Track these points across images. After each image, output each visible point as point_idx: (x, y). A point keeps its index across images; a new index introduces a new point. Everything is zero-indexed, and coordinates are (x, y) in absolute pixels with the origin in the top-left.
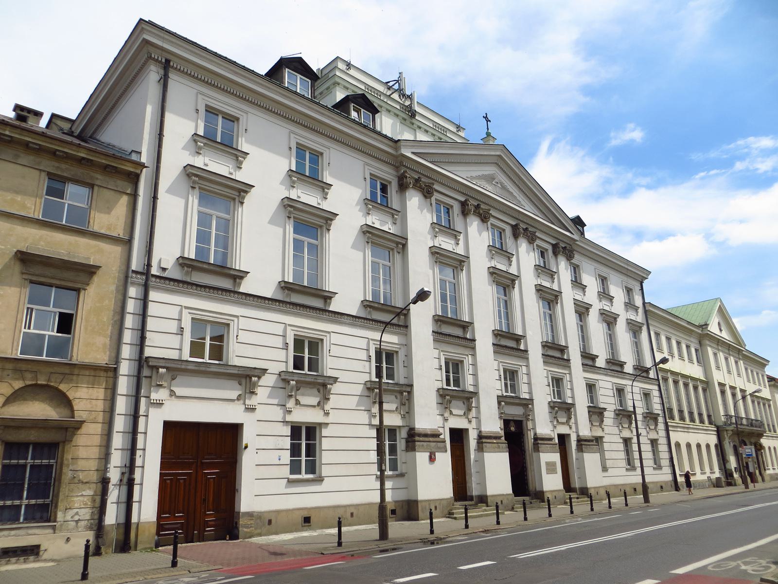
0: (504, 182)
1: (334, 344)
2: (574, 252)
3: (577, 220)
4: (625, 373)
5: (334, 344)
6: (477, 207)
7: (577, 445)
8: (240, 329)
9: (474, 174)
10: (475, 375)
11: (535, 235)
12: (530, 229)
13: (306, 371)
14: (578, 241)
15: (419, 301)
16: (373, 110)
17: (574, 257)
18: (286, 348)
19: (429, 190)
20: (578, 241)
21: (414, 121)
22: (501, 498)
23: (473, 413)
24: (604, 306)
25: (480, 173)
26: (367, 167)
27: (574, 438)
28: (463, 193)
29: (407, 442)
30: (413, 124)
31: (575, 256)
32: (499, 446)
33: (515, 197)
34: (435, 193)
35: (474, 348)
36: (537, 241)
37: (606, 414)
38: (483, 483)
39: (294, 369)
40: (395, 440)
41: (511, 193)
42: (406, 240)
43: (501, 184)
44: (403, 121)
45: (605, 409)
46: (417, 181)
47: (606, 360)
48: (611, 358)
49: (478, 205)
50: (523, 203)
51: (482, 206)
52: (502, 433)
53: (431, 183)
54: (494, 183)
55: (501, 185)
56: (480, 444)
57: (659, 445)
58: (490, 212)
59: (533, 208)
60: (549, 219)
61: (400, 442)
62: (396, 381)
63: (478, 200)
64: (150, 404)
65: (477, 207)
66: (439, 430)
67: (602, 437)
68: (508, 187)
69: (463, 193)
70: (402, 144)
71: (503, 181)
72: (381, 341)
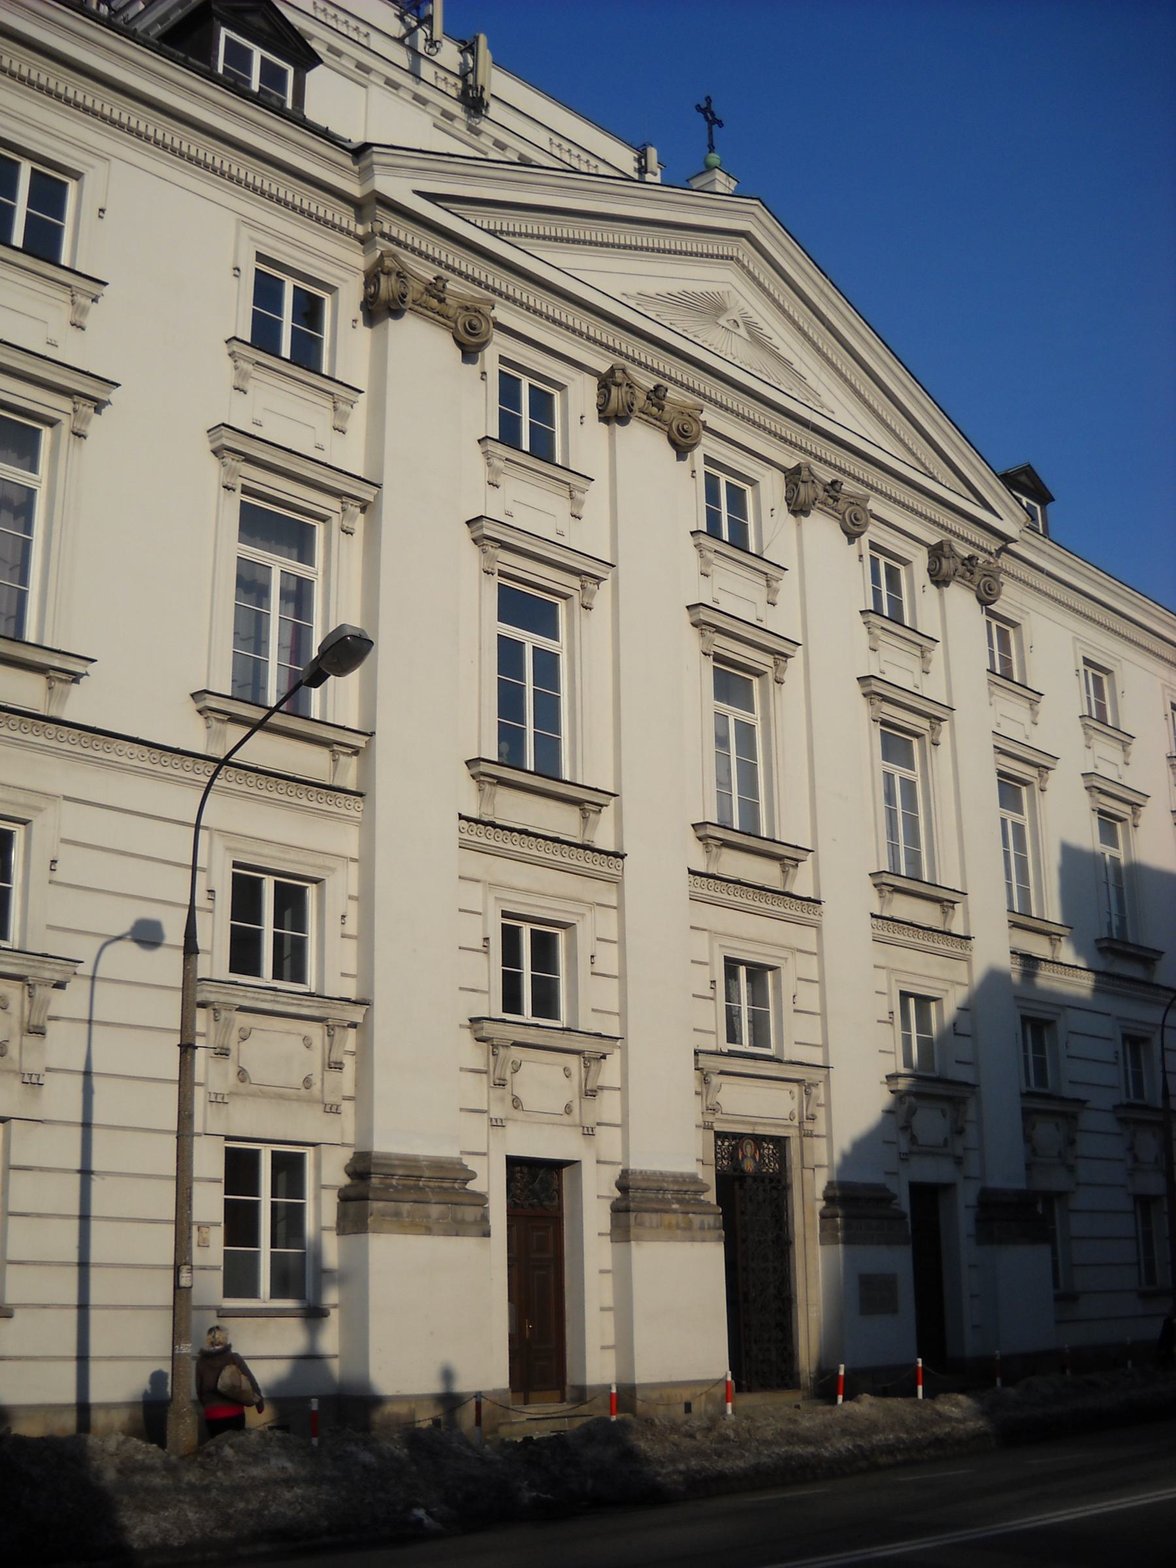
0: (762, 324)
1: (701, 963)
2: (1003, 578)
3: (1023, 478)
4: (1158, 986)
5: (701, 963)
6: (657, 395)
7: (978, 1221)
8: (706, 964)
9: (652, 287)
10: (366, 939)
11: (864, 509)
12: (849, 486)
13: (527, 1015)
14: (1015, 541)
15: (332, 677)
16: (306, 59)
17: (999, 593)
18: (887, 1019)
19: (475, 322)
20: (1015, 541)
21: (484, 125)
22: (686, 1395)
23: (609, 1106)
24: (1098, 762)
25: (675, 287)
26: (246, 231)
27: (967, 1196)
28: (607, 347)
29: (345, 1197)
30: (477, 132)
31: (1005, 589)
32: (690, 1222)
33: (801, 378)
34: (497, 337)
35: (616, 882)
36: (870, 528)
37: (1088, 1120)
38: (57, 1409)
39: (232, 970)
40: (299, 1192)
41: (786, 363)
42: (375, 490)
43: (751, 327)
44: (444, 122)
45: (1081, 1102)
46: (436, 290)
47: (1097, 941)
48: (1115, 937)
49: (658, 387)
50: (826, 398)
51: (674, 394)
52: (708, 1176)
53: (481, 301)
54: (722, 322)
55: (749, 332)
56: (621, 1214)
57: (11, 1270)
58: (703, 417)
59: (861, 418)
60: (918, 459)
61: (317, 1198)
62: (564, 1021)
63: (658, 373)
64: (209, 1104)
65: (657, 395)
66: (465, 1162)
67: (1062, 1195)
68: (776, 341)
69: (607, 347)
70: (376, 158)
71: (756, 319)
72: (1163, 1026)
